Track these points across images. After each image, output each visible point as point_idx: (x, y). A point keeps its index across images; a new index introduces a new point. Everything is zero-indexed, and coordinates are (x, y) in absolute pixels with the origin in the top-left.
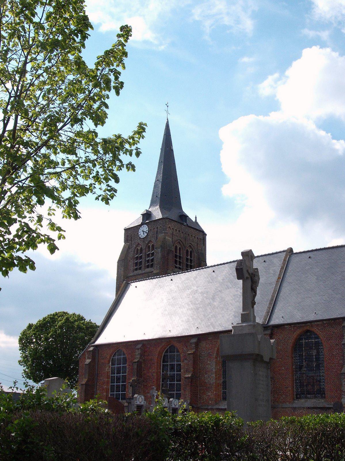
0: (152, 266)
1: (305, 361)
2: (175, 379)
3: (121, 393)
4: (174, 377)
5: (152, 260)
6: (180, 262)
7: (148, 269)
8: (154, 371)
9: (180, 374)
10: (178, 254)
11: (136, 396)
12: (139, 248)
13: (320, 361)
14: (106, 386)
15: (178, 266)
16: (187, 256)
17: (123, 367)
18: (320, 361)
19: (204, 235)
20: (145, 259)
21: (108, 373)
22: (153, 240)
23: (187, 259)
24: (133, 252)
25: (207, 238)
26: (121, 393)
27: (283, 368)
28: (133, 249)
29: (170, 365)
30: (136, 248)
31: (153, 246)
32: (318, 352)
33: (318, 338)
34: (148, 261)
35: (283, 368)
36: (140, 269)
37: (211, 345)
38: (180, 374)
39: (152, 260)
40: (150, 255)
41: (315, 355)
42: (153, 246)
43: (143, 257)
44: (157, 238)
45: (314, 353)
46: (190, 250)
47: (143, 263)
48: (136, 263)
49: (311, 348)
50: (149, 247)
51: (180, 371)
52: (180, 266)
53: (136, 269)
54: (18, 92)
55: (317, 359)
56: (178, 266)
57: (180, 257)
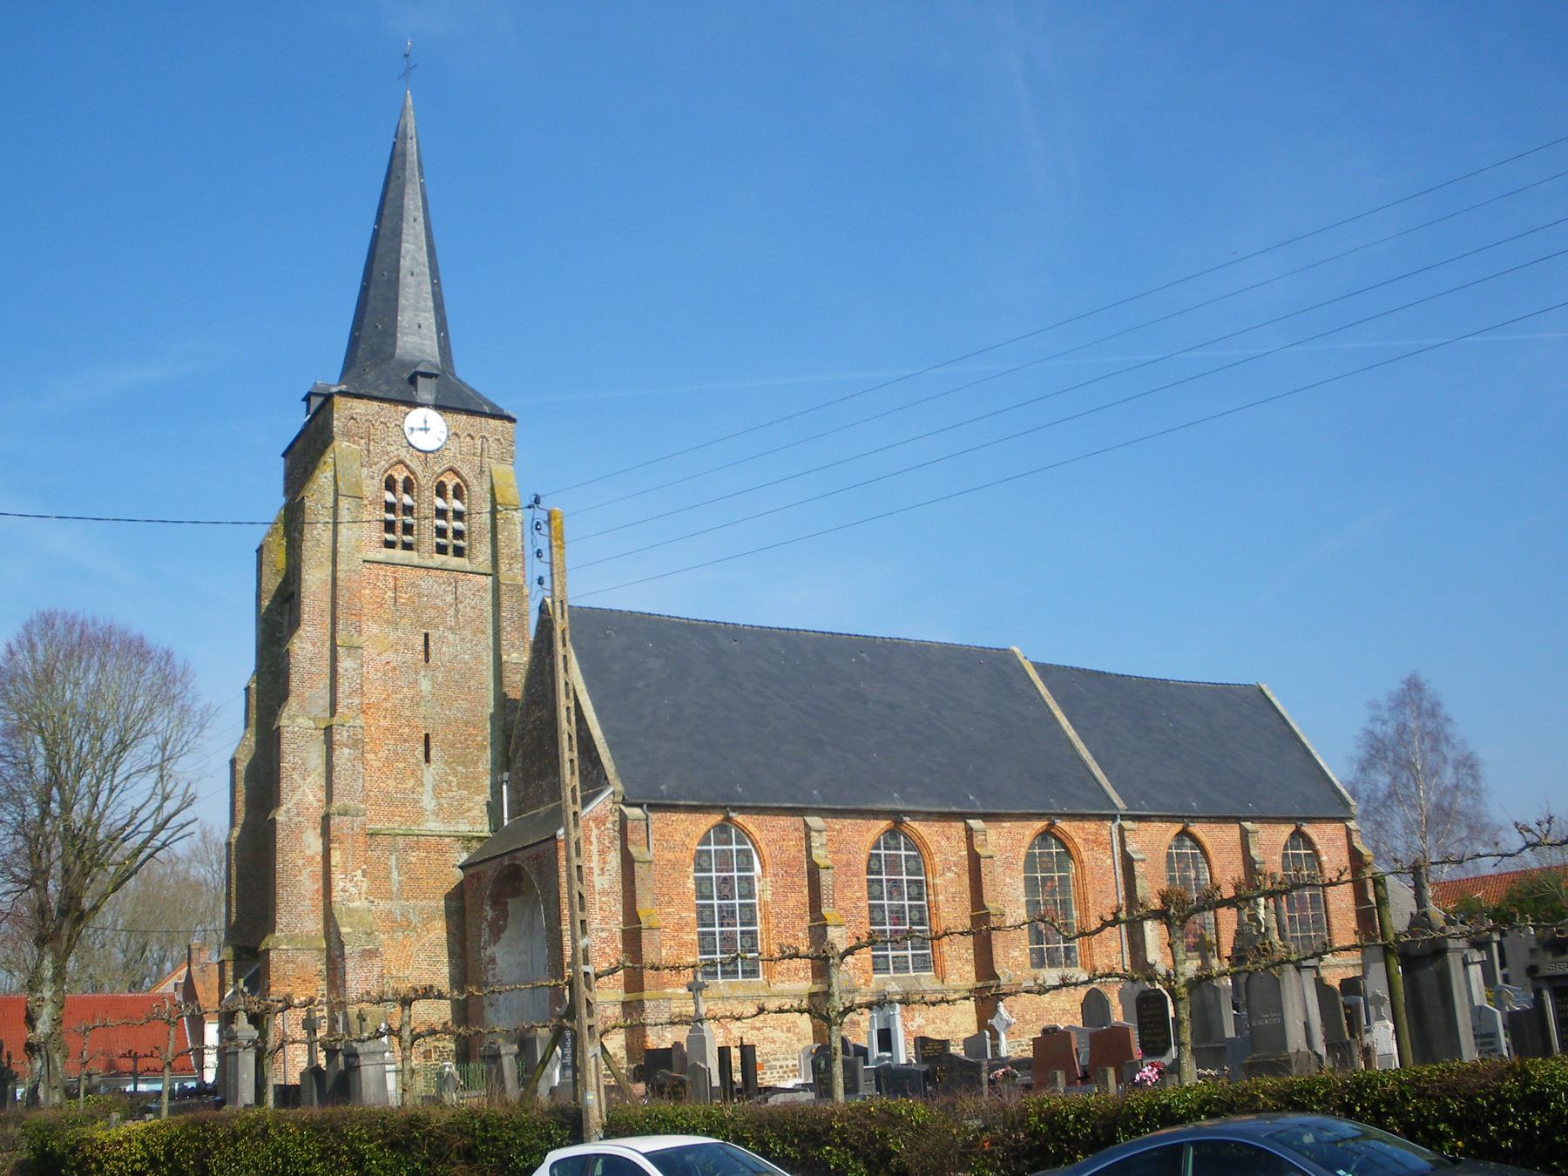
2: (904, 918)
8: (858, 894)
30: (386, 471)
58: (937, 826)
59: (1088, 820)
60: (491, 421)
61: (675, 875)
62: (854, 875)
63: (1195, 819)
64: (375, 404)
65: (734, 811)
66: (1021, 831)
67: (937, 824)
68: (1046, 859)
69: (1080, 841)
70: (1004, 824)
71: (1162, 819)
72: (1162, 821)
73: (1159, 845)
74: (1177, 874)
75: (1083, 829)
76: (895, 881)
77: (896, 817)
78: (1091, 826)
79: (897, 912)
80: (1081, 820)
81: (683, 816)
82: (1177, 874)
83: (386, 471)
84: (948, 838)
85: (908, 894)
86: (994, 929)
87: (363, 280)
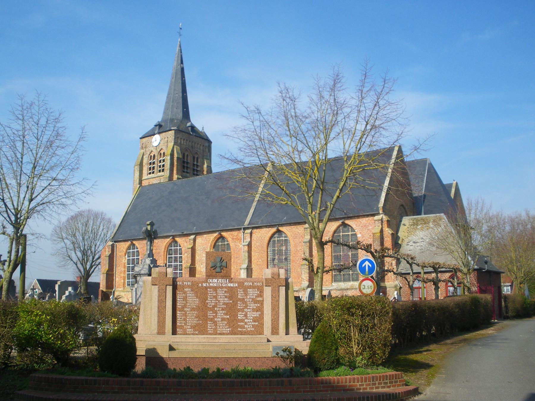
0: (163, 170)
1: (277, 255)
2: (178, 269)
3: (284, 239)
4: (177, 267)
5: (163, 166)
6: (187, 168)
7: (160, 173)
8: (161, 262)
9: (182, 265)
10: (186, 160)
11: (386, 268)
12: (152, 155)
13: (288, 254)
14: (123, 275)
15: (185, 170)
16: (194, 161)
17: (136, 259)
18: (288, 254)
19: (210, 142)
20: (158, 165)
21: (124, 264)
22: (164, 148)
23: (194, 164)
24: (147, 158)
25: (213, 145)
26: (350, 233)
27: (260, 260)
28: (147, 155)
29: (174, 257)
30: (150, 154)
31: (164, 153)
32: (287, 249)
33: (286, 237)
34: (160, 166)
35: (260, 260)
36: (153, 173)
37: (205, 241)
38: (182, 265)
39: (163, 166)
40: (162, 161)
41: (285, 250)
42: (164, 153)
43: (156, 163)
44: (167, 147)
45: (284, 248)
46: (196, 156)
47: (156, 168)
48: (150, 168)
49: (282, 245)
50: (161, 154)
51: (182, 262)
52: (187, 171)
53: (150, 173)
54: (119, 290)
55: (286, 254)
56: (185, 170)
57: (187, 163)
58: (184, 239)
59: (234, 231)
60: (169, 132)
61: (121, 259)
62: (160, 256)
63: (282, 225)
64: (147, 138)
65: (223, 232)
66: (209, 237)
67: (184, 238)
68: (223, 246)
69: (230, 239)
70: (204, 236)
71: (266, 227)
72: (267, 228)
73: (264, 238)
74: (276, 249)
75: (232, 234)
76: (176, 257)
77: (174, 237)
78: (235, 233)
79: (176, 267)
80: (231, 231)
81: (123, 243)
82: (276, 249)
83: (150, 154)
84: (187, 242)
85: (179, 261)
86: (387, 271)
87: (186, 96)
